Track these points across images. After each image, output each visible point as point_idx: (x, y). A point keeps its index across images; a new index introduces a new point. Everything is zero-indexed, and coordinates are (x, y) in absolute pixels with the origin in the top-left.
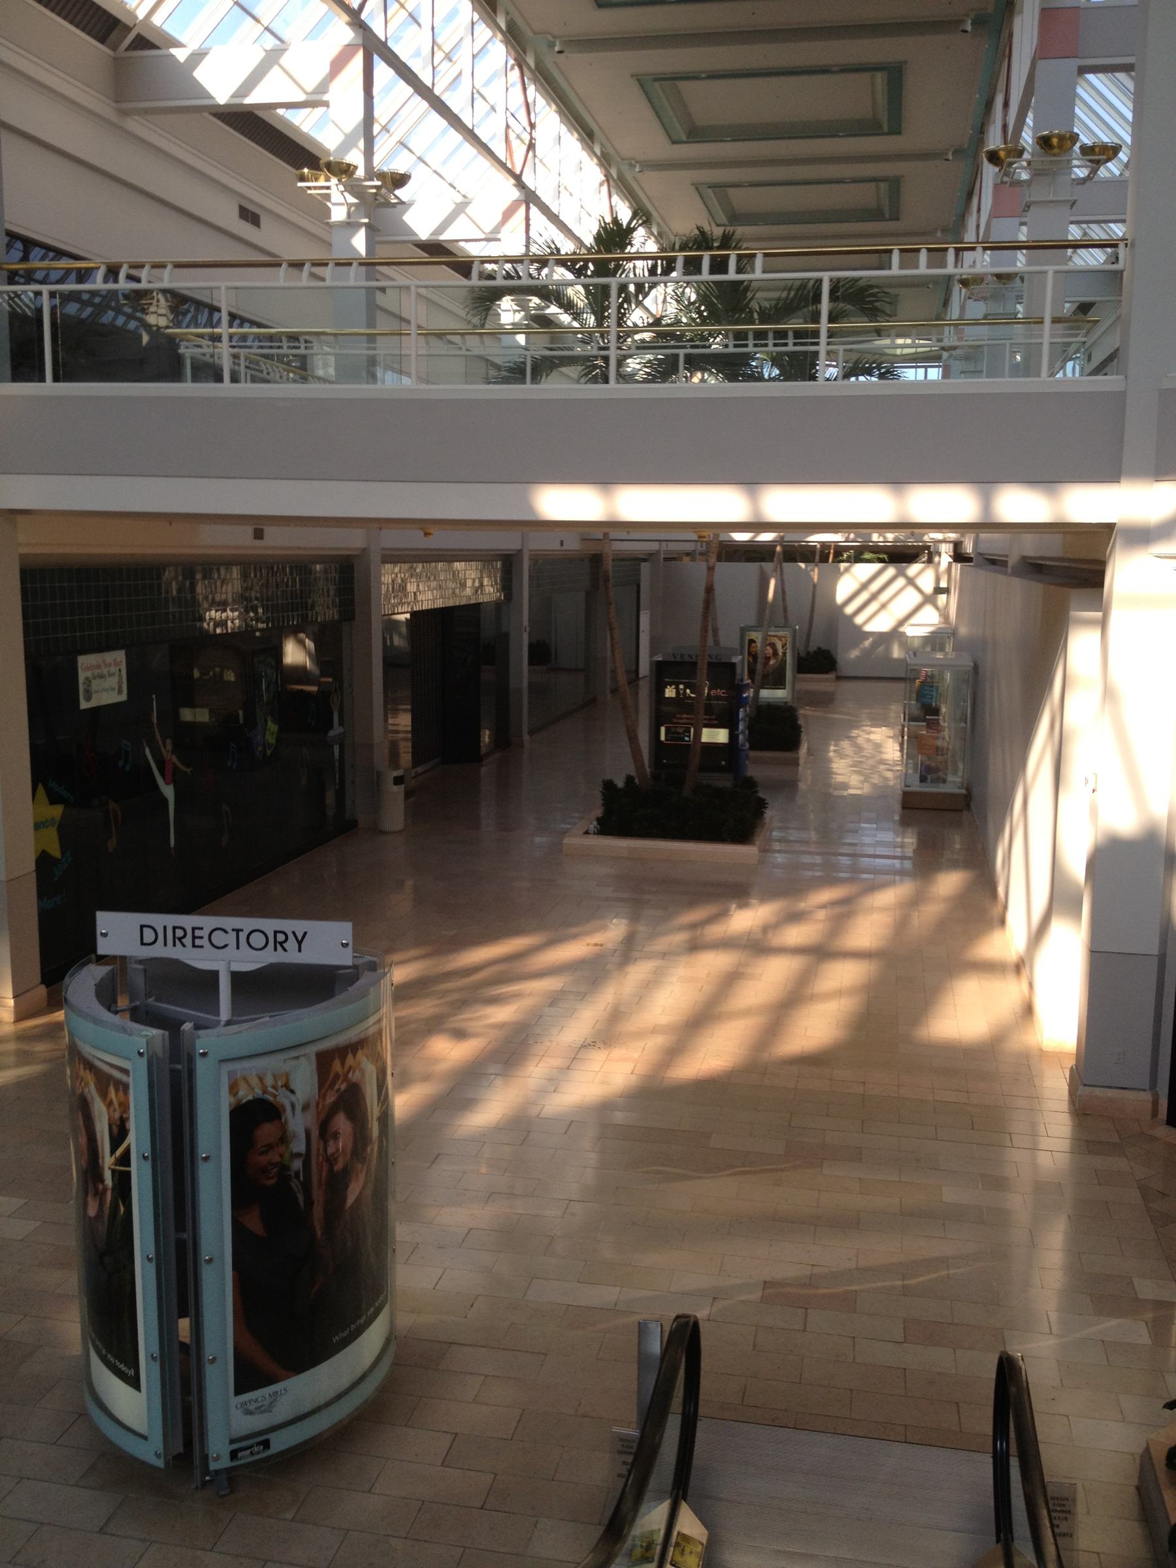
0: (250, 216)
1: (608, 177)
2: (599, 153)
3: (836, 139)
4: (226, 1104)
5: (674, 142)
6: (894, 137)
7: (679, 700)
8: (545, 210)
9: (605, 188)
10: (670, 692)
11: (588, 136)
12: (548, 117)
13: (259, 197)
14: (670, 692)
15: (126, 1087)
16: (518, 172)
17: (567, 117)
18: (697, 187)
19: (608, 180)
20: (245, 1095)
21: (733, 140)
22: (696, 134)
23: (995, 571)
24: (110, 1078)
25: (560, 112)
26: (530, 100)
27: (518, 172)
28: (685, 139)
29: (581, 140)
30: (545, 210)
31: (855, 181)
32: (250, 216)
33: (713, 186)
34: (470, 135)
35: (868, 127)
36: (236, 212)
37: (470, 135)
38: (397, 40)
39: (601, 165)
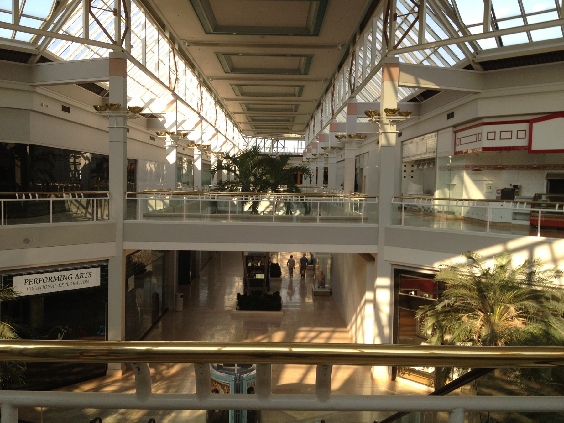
0: (66, 109)
1: (173, 48)
2: (168, 37)
3: (288, 37)
4: (247, 388)
5: (207, 33)
6: (315, 37)
7: (253, 266)
8: (184, 102)
9: (172, 54)
10: (250, 264)
11: (162, 26)
12: (182, 65)
13: (69, 101)
14: (250, 264)
15: (229, 387)
16: (172, 89)
17: (149, 15)
18: (217, 54)
19: (173, 50)
20: (249, 386)
21: (236, 34)
22: (218, 29)
23: (392, 274)
24: (225, 385)
25: (146, 13)
26: (176, 61)
27: (172, 89)
28: (212, 32)
29: (158, 29)
30: (184, 102)
31: (292, 56)
32: (66, 109)
33: (224, 54)
34: (158, 80)
35: (304, 31)
36: (61, 108)
37: (158, 80)
38: (108, 28)
39: (169, 42)
